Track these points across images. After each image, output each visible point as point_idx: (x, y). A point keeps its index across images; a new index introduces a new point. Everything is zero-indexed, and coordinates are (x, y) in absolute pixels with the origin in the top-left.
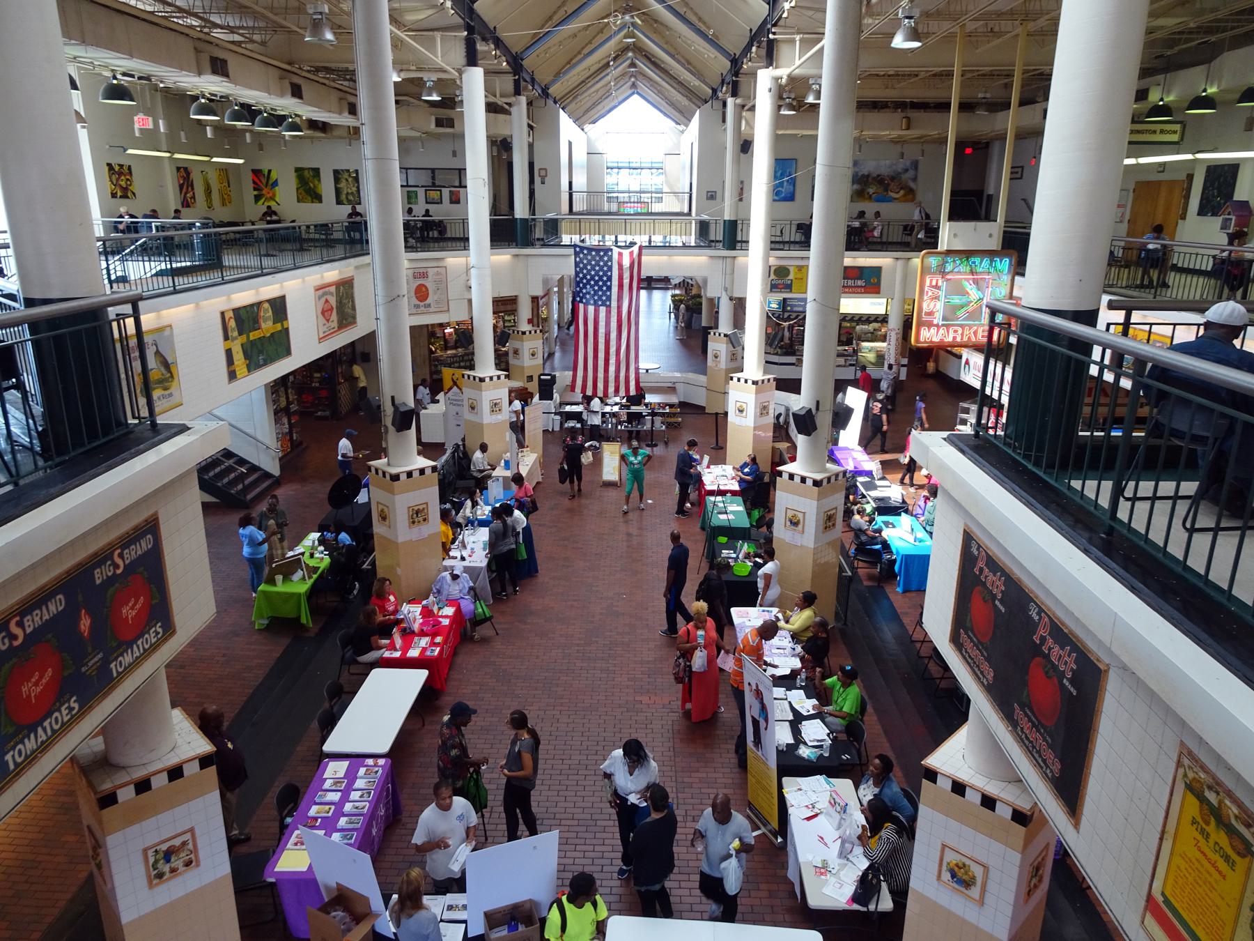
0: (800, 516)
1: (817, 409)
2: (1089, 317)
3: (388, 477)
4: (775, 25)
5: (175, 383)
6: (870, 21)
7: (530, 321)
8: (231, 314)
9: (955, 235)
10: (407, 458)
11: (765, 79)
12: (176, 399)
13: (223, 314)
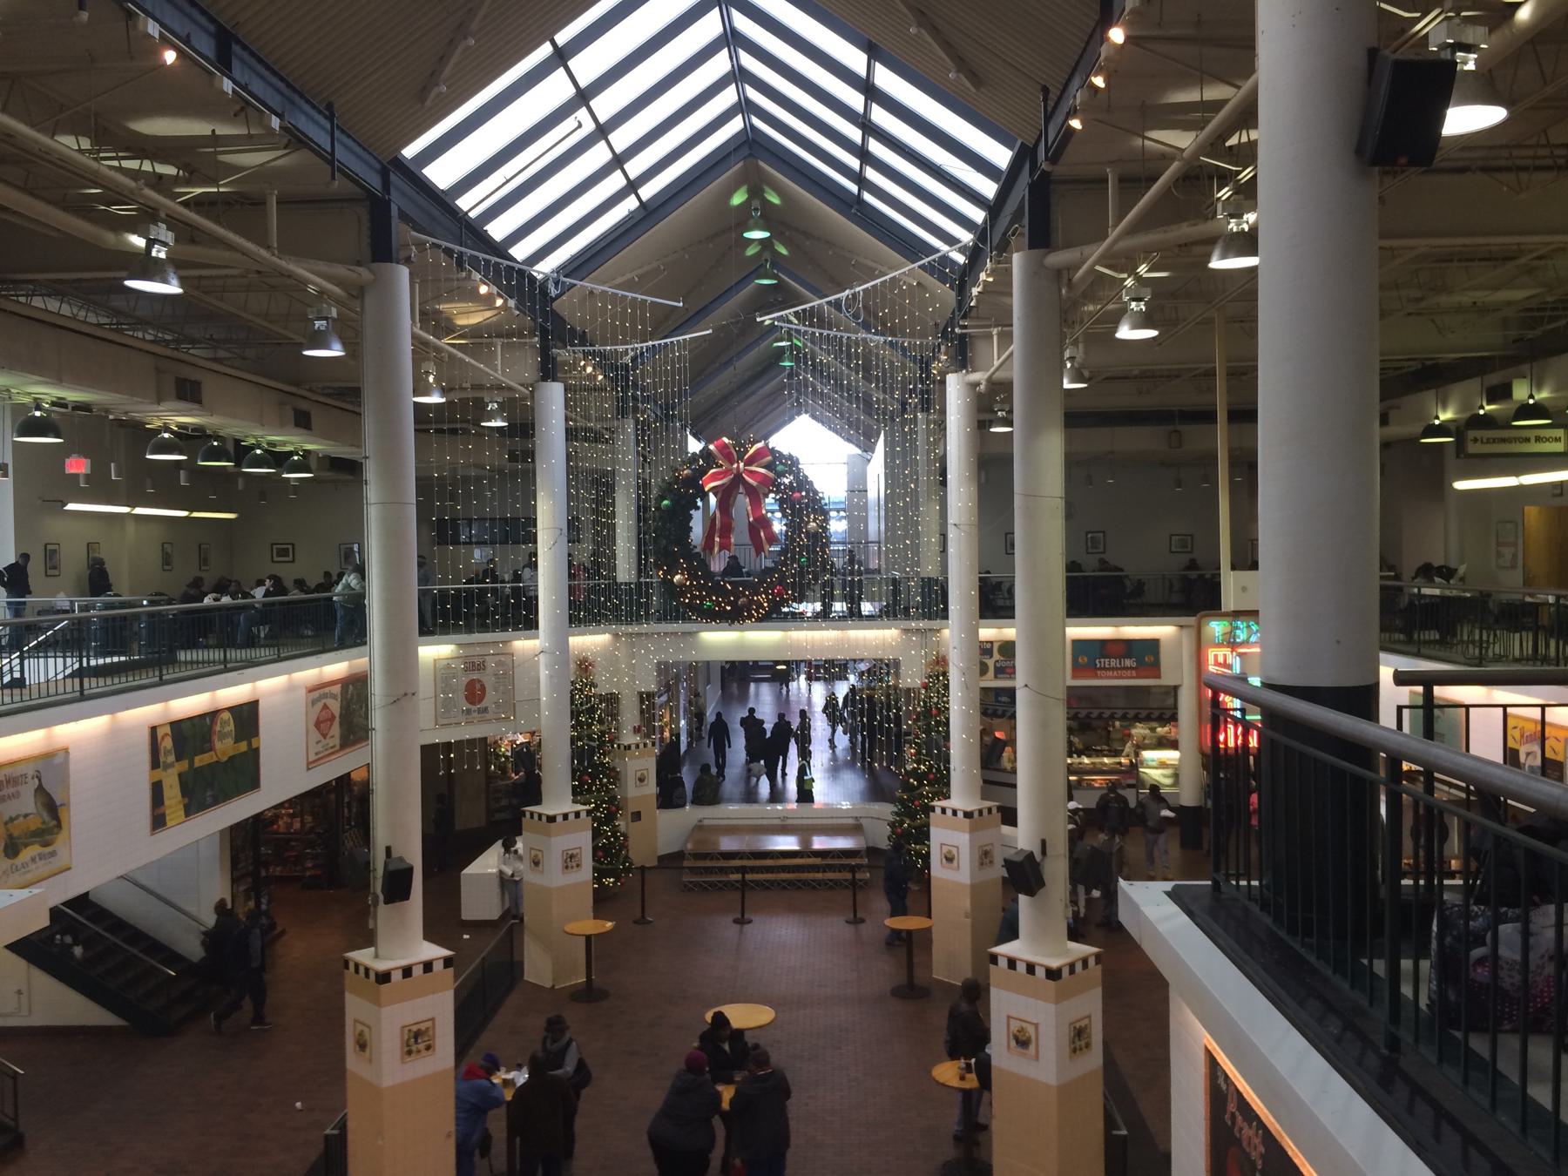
0: (1031, 1030)
1: (1044, 852)
2: (1363, 700)
3: (372, 975)
4: (964, 317)
5: (64, 832)
6: (1091, 308)
7: (637, 730)
8: (168, 730)
9: (1244, 589)
10: (404, 942)
11: (955, 388)
12: (61, 860)
13: (154, 729)
